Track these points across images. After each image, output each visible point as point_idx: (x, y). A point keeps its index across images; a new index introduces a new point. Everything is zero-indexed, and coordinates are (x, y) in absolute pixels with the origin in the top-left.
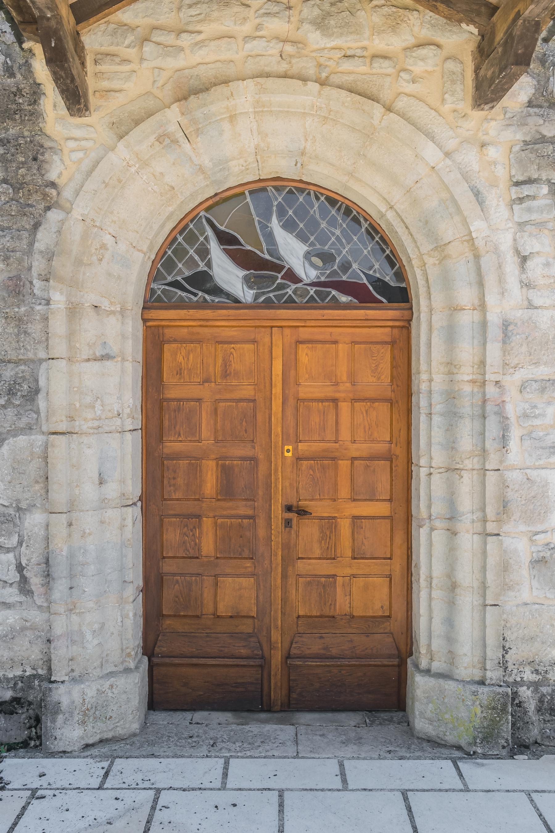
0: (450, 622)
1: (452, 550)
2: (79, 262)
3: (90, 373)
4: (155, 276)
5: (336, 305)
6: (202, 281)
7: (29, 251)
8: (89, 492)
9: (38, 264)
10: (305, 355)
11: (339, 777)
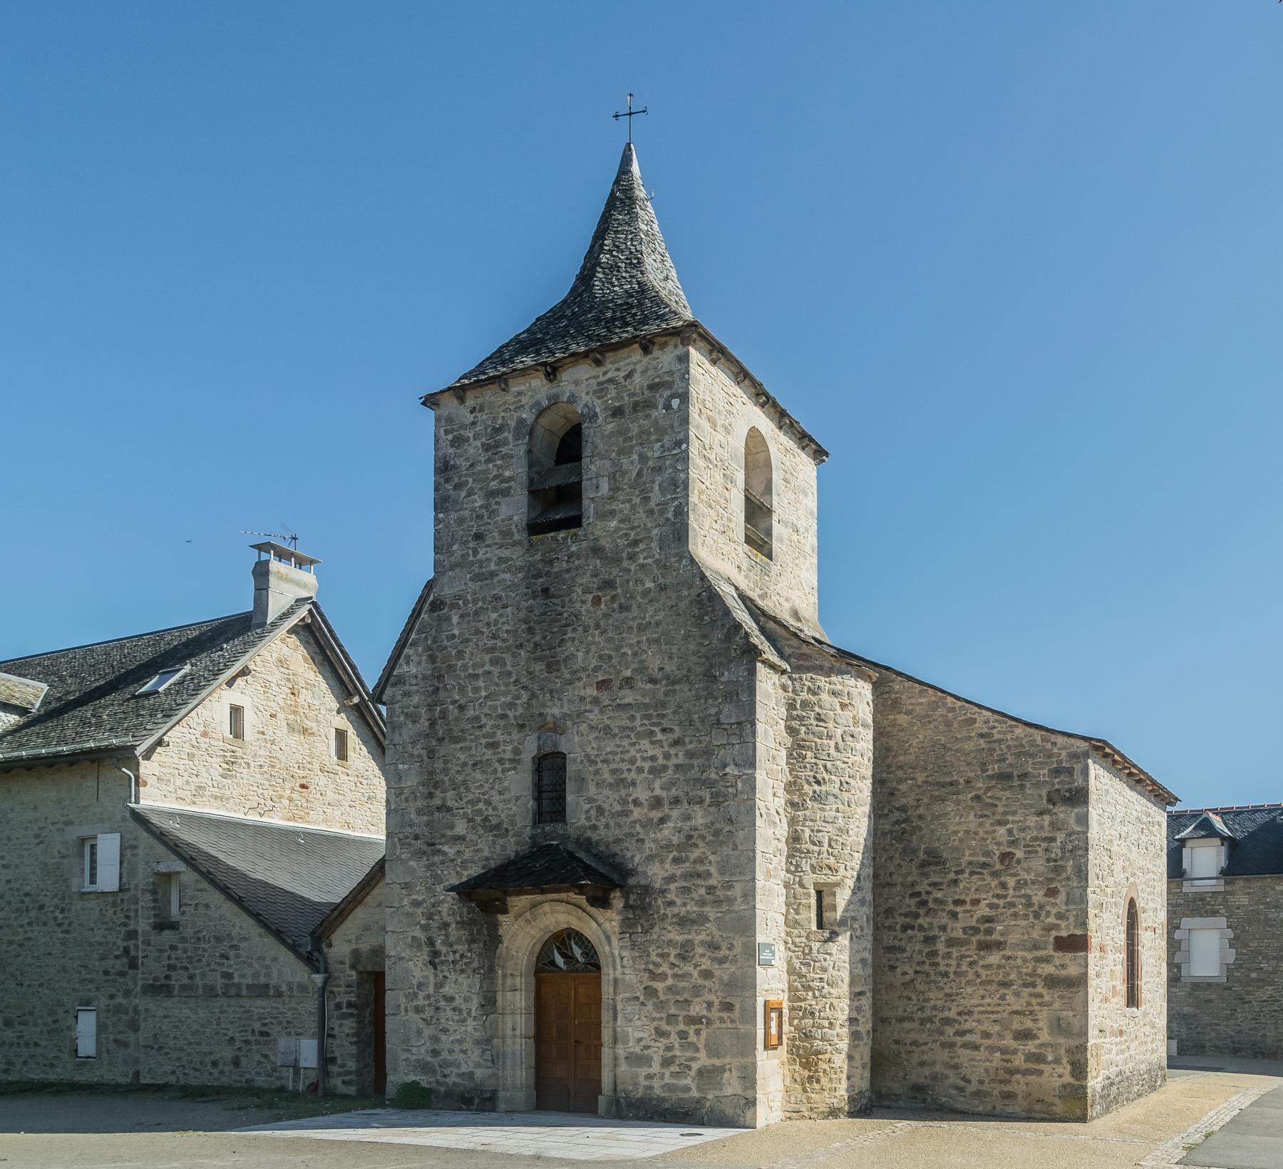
5: (590, 971)
6: (553, 963)
8: (509, 1032)
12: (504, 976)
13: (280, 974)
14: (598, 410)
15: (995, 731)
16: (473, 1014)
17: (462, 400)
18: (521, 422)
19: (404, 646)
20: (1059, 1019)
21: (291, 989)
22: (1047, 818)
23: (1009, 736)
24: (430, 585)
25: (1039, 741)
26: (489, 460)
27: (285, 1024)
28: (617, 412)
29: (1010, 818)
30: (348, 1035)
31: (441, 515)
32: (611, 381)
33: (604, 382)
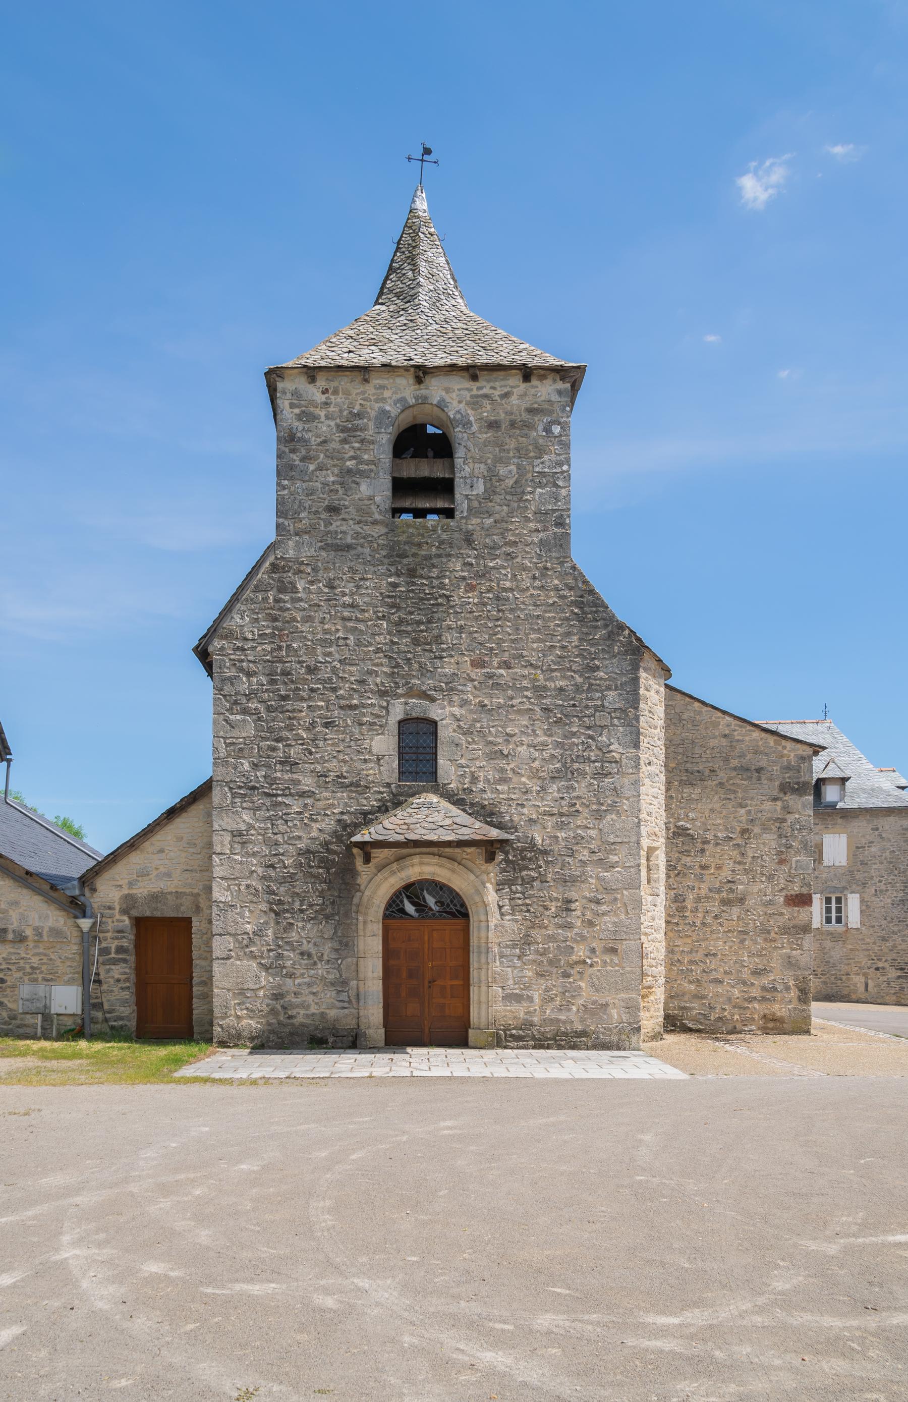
0: (479, 1013)
1: (479, 992)
2: (366, 908)
3: (370, 940)
4: (386, 909)
6: (403, 911)
7: (351, 904)
8: (370, 974)
9: (354, 908)
10: (435, 934)
11: (450, 1075)
12: (365, 922)
13: (23, 918)
14: (472, 418)
15: (736, 733)
16: (325, 957)
17: (312, 380)
18: (383, 413)
19: (237, 600)
20: (789, 957)
21: (40, 935)
22: (779, 803)
23: (747, 738)
24: (272, 547)
25: (772, 744)
26: (344, 441)
27: (28, 970)
28: (493, 425)
29: (749, 802)
30: (118, 980)
31: (286, 482)
32: (486, 396)
33: (477, 396)
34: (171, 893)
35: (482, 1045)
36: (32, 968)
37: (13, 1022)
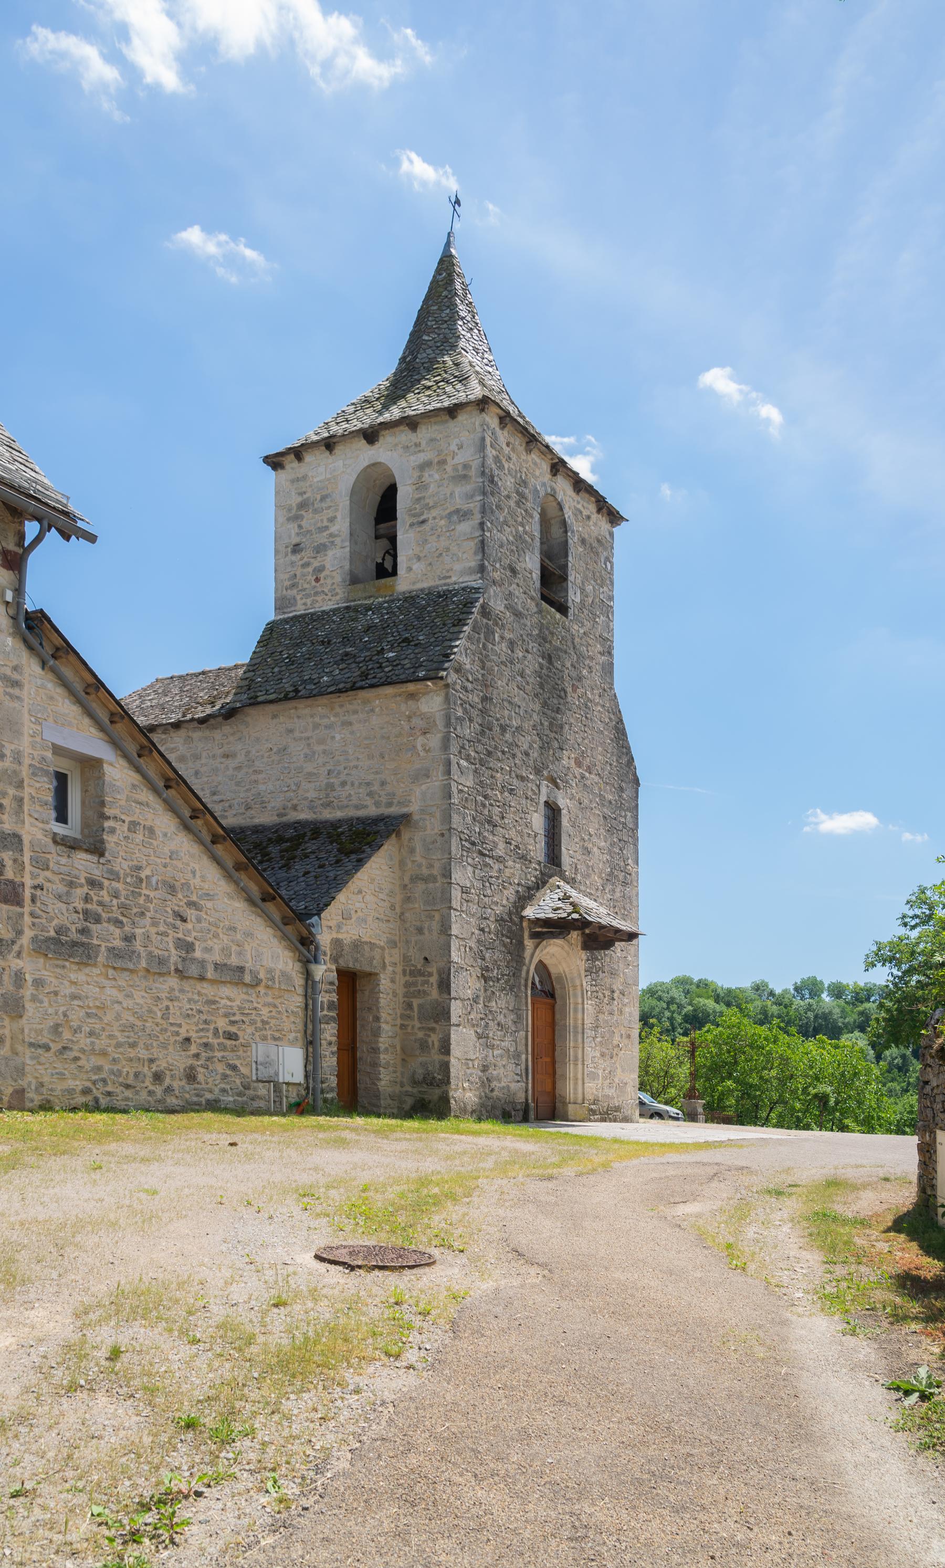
0: (575, 1089)
34: (366, 943)
35: (581, 1118)
36: (263, 1021)
37: (247, 1092)
